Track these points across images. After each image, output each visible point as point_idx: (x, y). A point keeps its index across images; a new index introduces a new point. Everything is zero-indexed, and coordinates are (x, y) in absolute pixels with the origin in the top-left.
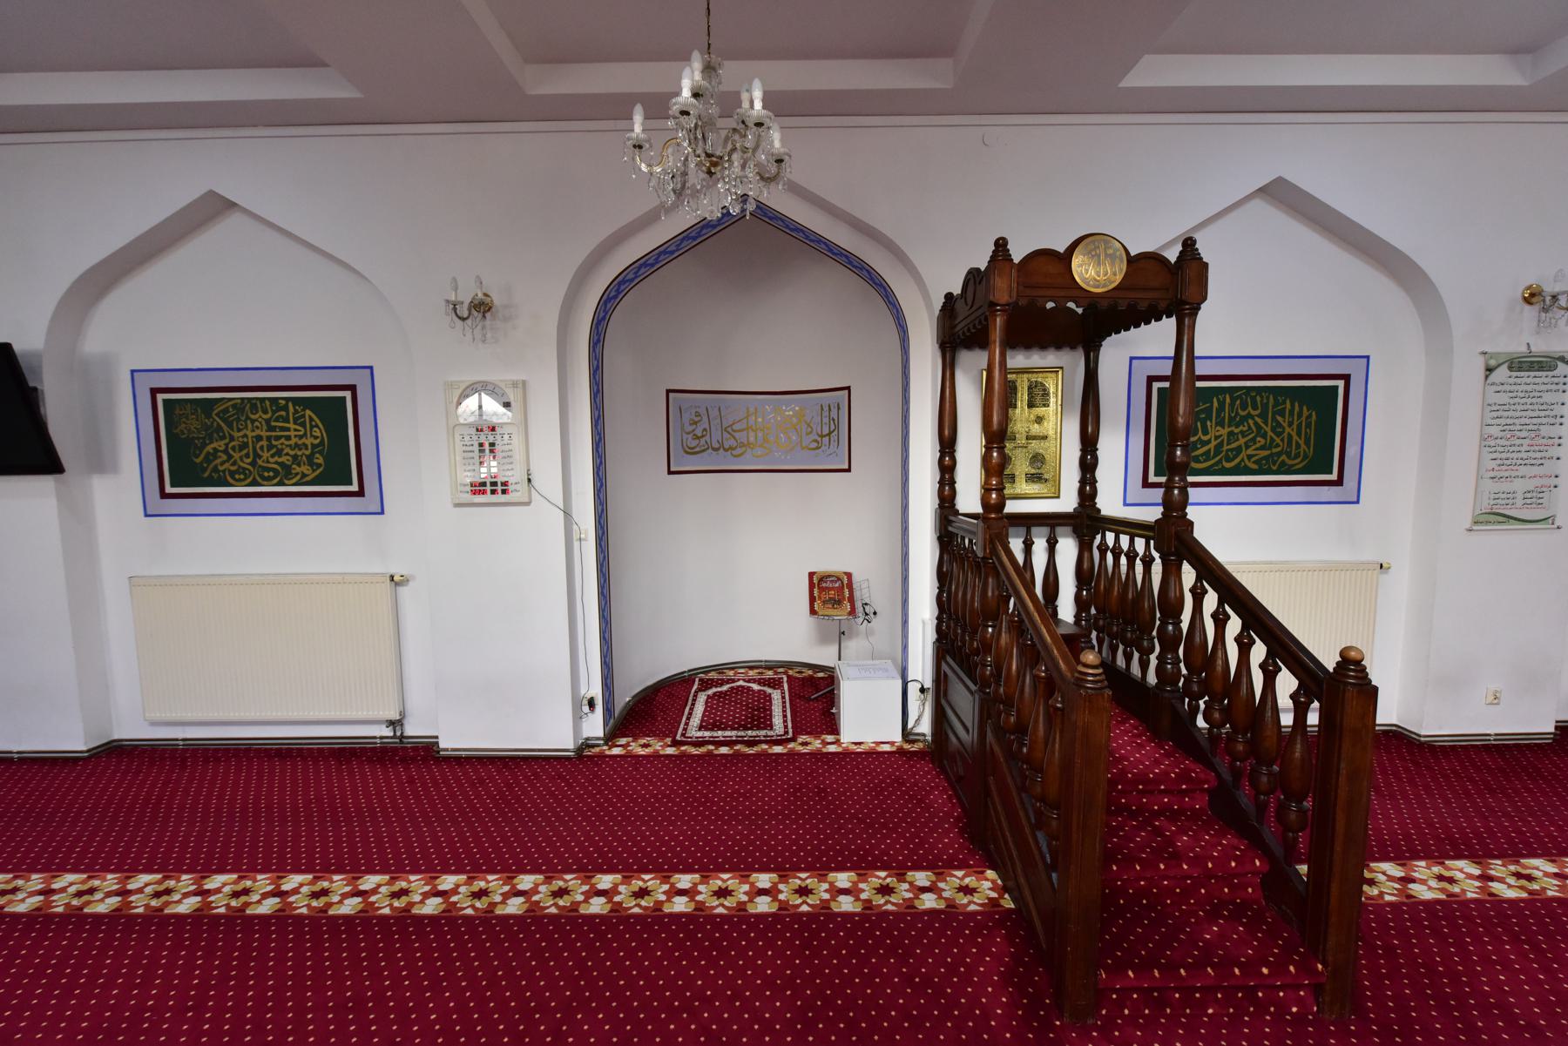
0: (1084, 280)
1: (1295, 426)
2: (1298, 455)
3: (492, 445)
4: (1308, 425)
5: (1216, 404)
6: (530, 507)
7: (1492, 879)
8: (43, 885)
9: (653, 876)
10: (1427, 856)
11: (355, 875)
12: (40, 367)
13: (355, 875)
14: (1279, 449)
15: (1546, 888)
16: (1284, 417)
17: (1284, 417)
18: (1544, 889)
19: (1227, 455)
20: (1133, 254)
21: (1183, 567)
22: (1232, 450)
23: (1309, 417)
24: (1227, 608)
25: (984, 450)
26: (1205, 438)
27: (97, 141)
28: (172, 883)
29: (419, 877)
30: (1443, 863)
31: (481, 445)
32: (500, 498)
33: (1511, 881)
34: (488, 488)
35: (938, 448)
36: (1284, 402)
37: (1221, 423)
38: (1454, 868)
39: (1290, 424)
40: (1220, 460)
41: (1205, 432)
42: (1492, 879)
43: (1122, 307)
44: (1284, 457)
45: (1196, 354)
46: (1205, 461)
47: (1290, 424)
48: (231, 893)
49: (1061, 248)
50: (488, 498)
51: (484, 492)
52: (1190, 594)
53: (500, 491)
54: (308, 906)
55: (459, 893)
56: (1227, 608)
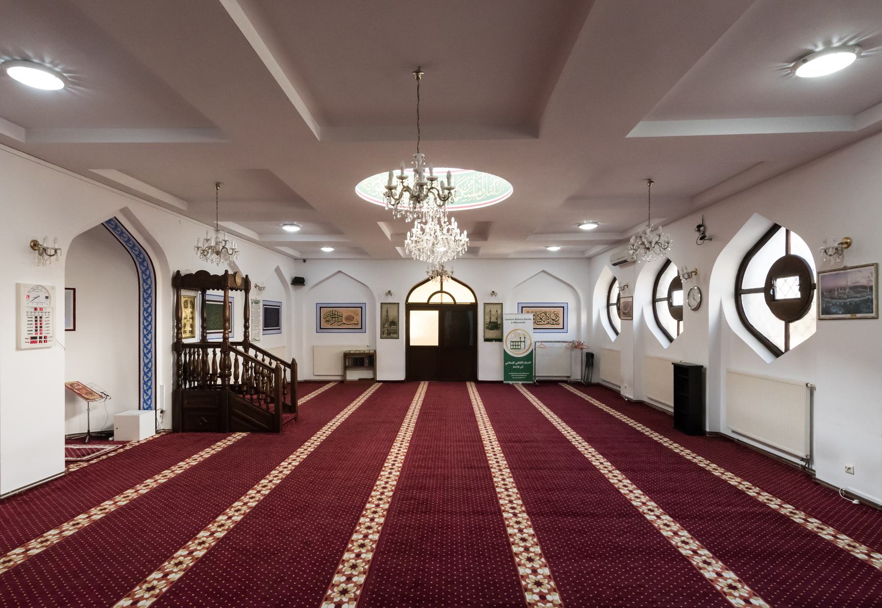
3: (41, 317)
6: (879, 320)
7: (157, 480)
8: (167, 588)
9: (716, 586)
10: (118, 494)
11: (711, 582)
12: (172, 350)
13: (711, 582)
15: (140, 589)
18: (140, 485)
20: (412, 344)
28: (725, 590)
29: (716, 586)
30: (196, 538)
31: (36, 317)
32: (43, 345)
33: (144, 488)
34: (38, 340)
38: (179, 572)
42: (157, 480)
48: (736, 591)
50: (38, 345)
51: (35, 342)
53: (38, 342)
54: (743, 587)
55: (740, 594)
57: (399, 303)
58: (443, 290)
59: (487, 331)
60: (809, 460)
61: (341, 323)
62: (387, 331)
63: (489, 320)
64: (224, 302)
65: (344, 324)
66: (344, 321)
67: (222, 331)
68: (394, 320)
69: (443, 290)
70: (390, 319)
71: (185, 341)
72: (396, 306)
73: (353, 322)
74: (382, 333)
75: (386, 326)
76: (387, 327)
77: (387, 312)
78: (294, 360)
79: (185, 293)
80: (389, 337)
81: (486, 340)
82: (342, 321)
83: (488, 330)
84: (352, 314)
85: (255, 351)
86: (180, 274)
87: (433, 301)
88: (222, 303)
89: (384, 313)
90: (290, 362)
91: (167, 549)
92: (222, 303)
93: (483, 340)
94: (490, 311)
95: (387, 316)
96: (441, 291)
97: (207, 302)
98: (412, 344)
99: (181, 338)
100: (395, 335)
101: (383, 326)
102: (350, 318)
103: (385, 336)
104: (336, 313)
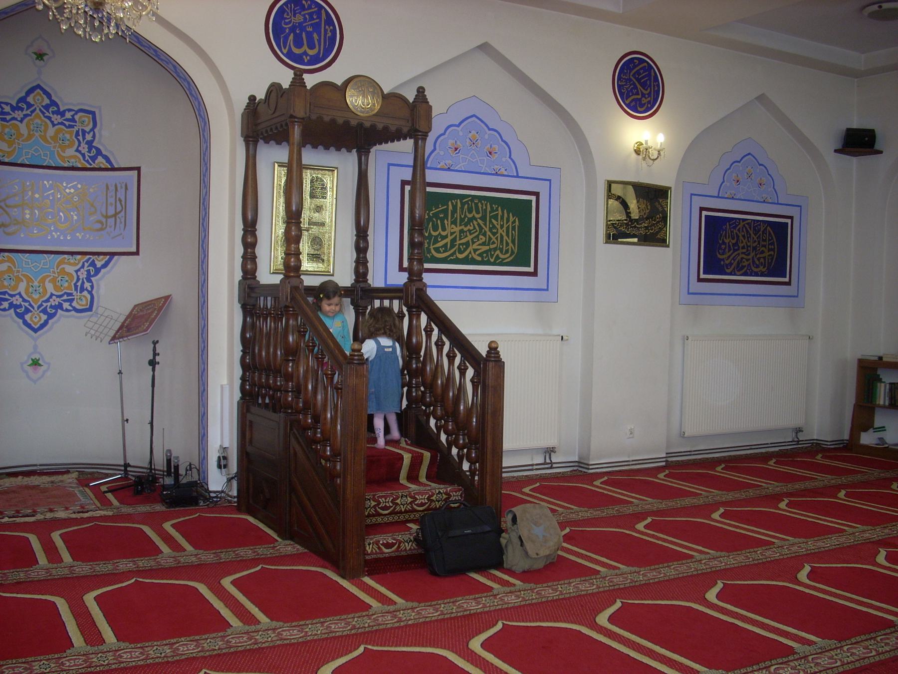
1: (505, 228)
2: (507, 252)
4: (514, 228)
5: (450, 207)
14: (495, 246)
22: (462, 244)
23: (514, 222)
26: (444, 234)
37: (454, 222)
39: (502, 227)
40: (454, 253)
41: (444, 229)
44: (498, 252)
46: (444, 252)
47: (502, 227)
97: (429, 189)
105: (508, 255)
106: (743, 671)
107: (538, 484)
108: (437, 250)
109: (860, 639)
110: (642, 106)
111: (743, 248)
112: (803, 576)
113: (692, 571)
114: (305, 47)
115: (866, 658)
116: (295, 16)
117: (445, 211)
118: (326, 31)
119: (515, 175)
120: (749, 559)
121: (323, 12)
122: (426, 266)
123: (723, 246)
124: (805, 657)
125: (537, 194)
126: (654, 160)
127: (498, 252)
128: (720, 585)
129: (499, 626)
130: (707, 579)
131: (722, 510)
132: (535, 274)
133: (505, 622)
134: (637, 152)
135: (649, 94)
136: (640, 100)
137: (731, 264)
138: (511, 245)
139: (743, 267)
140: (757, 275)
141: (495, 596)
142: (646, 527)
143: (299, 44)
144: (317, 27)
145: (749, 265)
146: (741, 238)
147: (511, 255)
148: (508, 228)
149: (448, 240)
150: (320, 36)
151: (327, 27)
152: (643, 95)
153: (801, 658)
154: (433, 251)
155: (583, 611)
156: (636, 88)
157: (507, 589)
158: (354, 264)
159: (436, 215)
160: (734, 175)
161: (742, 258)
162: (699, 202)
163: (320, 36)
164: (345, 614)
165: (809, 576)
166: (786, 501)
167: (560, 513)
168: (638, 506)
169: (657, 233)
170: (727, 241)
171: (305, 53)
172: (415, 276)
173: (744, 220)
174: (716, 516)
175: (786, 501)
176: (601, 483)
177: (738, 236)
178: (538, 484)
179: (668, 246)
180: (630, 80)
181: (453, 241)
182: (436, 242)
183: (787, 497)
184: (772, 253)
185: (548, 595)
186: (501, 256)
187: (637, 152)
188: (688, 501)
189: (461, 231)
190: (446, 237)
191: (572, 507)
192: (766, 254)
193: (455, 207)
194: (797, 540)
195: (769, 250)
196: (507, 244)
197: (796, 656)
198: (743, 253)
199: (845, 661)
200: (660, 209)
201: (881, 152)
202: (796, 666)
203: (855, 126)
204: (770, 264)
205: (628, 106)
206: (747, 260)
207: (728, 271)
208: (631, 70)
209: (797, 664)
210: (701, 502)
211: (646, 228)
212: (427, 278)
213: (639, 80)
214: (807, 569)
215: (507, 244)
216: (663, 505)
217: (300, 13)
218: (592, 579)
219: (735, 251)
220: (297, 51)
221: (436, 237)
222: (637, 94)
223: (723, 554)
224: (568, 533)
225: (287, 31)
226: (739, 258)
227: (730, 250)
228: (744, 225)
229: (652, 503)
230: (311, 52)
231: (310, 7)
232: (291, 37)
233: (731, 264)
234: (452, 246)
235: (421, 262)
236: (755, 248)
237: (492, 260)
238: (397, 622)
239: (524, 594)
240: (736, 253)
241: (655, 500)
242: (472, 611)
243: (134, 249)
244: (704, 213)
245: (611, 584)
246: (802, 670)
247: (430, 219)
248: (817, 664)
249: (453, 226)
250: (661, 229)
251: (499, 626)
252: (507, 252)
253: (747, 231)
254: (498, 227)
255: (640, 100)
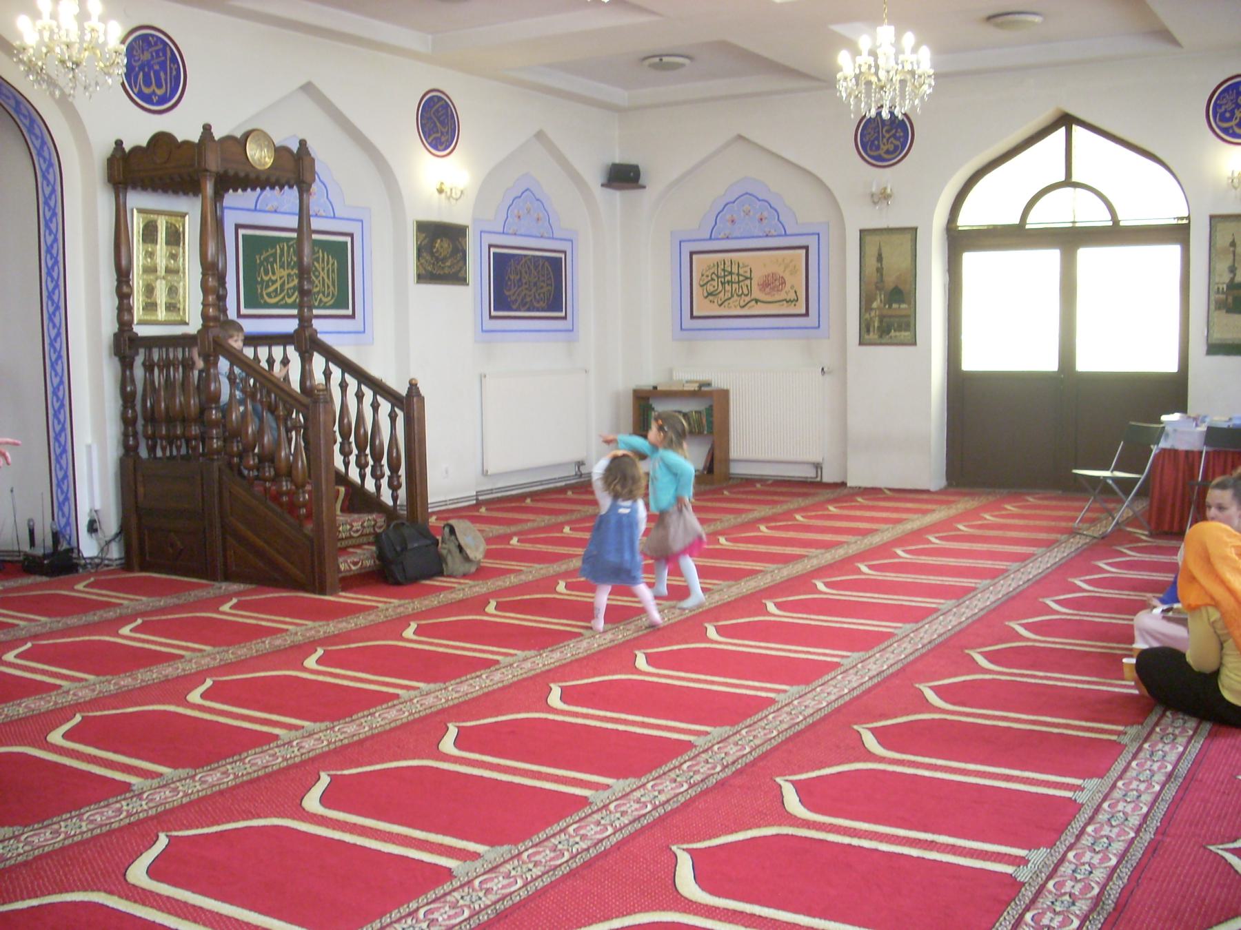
0: (253, 159)
1: (326, 271)
2: (328, 295)
4: (333, 271)
5: (278, 251)
14: (318, 289)
16: (318, 262)
17: (318, 262)
19: (288, 294)
21: (220, 364)
22: (290, 288)
23: (333, 264)
24: (396, 409)
25: (131, 277)
26: (274, 278)
27: (715, 329)
35: (115, 277)
36: (318, 252)
37: (282, 266)
39: (323, 269)
40: (284, 298)
41: (274, 273)
43: (242, 174)
44: (321, 295)
45: (297, 217)
46: (275, 297)
47: (323, 269)
49: (238, 135)
52: (227, 381)
56: (396, 409)
57: (916, 229)
58: (1075, 179)
59: (1222, 317)
60: (1216, 673)
61: (748, 299)
62: (881, 321)
63: (1226, 278)
64: (299, 230)
65: (757, 301)
66: (756, 293)
67: (295, 312)
68: (901, 287)
69: (1075, 179)
70: (890, 281)
71: (142, 331)
72: (909, 236)
73: (782, 296)
74: (865, 327)
75: (875, 305)
76: (879, 308)
77: (880, 258)
78: (413, 387)
79: (136, 200)
80: (884, 341)
81: (1215, 349)
82: (750, 291)
83: (1223, 313)
84: (780, 271)
85: (324, 360)
86: (123, 149)
87: (1036, 220)
88: (295, 235)
89: (872, 262)
90: (403, 390)
91: (21, 891)
92: (295, 235)
93: (1204, 348)
94: (1233, 244)
95: (880, 270)
96: (1068, 182)
97: (315, 236)
98: (969, 363)
99: (131, 323)
100: (904, 335)
101: (866, 302)
102: (772, 283)
103: (873, 336)
104: (735, 270)
105: (329, 298)
106: (377, 924)
107: (29, 645)
108: (269, 295)
109: (583, 815)
110: (441, 144)
111: (526, 283)
112: (448, 745)
113: (279, 763)
114: (154, 86)
115: (604, 839)
116: (143, 53)
117: (274, 255)
118: (171, 69)
119: (332, 215)
120: (441, 699)
121: (168, 49)
122: (315, 312)
123: (509, 283)
124: (606, 807)
125: (352, 235)
126: (457, 200)
127: (321, 295)
128: (325, 779)
129: (163, 841)
130: (302, 773)
131: (320, 652)
132: (353, 316)
133: (169, 834)
134: (441, 191)
135: (447, 132)
136: (440, 139)
137: (516, 300)
138: (331, 288)
139: (526, 303)
140: (538, 310)
141: (139, 796)
142: (204, 696)
143: (148, 84)
144: (163, 65)
145: (531, 300)
146: (524, 274)
147: (332, 298)
148: (328, 271)
149: (278, 284)
150: (166, 74)
151: (172, 65)
152: (442, 133)
153: (462, 886)
154: (265, 296)
155: (84, 873)
156: (435, 125)
157: (155, 782)
158: (116, 311)
159: (266, 259)
160: (516, 211)
161: (525, 295)
162: (489, 240)
163: (166, 74)
164: (113, 797)
165: (458, 743)
166: (413, 626)
167: (188, 658)
168: (296, 634)
169: (460, 271)
170: (512, 277)
171: (154, 93)
172: (305, 322)
173: (525, 256)
174: (311, 662)
175: (413, 626)
176: (17, 656)
177: (521, 273)
178: (29, 645)
179: (468, 285)
180: (431, 118)
181: (282, 285)
182: (268, 286)
183: (493, 598)
184: (550, 288)
185: (108, 822)
186: (325, 300)
187: (441, 191)
188: (266, 644)
189: (289, 275)
190: (274, 282)
191: (307, 622)
192: (545, 290)
193: (282, 250)
194: (432, 686)
195: (548, 285)
196: (328, 287)
197: (456, 883)
198: (526, 289)
199: (477, 907)
200: (460, 248)
201: (644, 187)
202: (458, 902)
203: (617, 161)
204: (548, 299)
205: (430, 144)
206: (530, 296)
207: (514, 307)
208: (432, 107)
209: (459, 897)
210: (382, 618)
211: (450, 267)
212: (317, 324)
213: (438, 119)
214: (453, 731)
215: (328, 287)
216: (231, 654)
217: (148, 50)
218: (273, 748)
219: (519, 287)
220: (146, 91)
221: (268, 282)
222: (437, 132)
223: (323, 725)
224: (80, 722)
225: (137, 69)
226: (523, 294)
227: (515, 286)
228: (526, 262)
229: (213, 654)
230: (160, 92)
231: (156, 44)
232: (141, 75)
233: (516, 300)
234: (282, 290)
235: (311, 308)
236: (535, 284)
237: (316, 304)
238: (126, 817)
239: (66, 826)
240: (520, 289)
241: (217, 649)
242: (56, 845)
243: (695, 314)
244: (492, 250)
245: (151, 805)
246: (465, 905)
247: (261, 263)
248: (583, 837)
249: (282, 270)
250: (461, 269)
251: (163, 841)
252: (328, 295)
253: (529, 268)
254: (320, 270)
255: (440, 139)
